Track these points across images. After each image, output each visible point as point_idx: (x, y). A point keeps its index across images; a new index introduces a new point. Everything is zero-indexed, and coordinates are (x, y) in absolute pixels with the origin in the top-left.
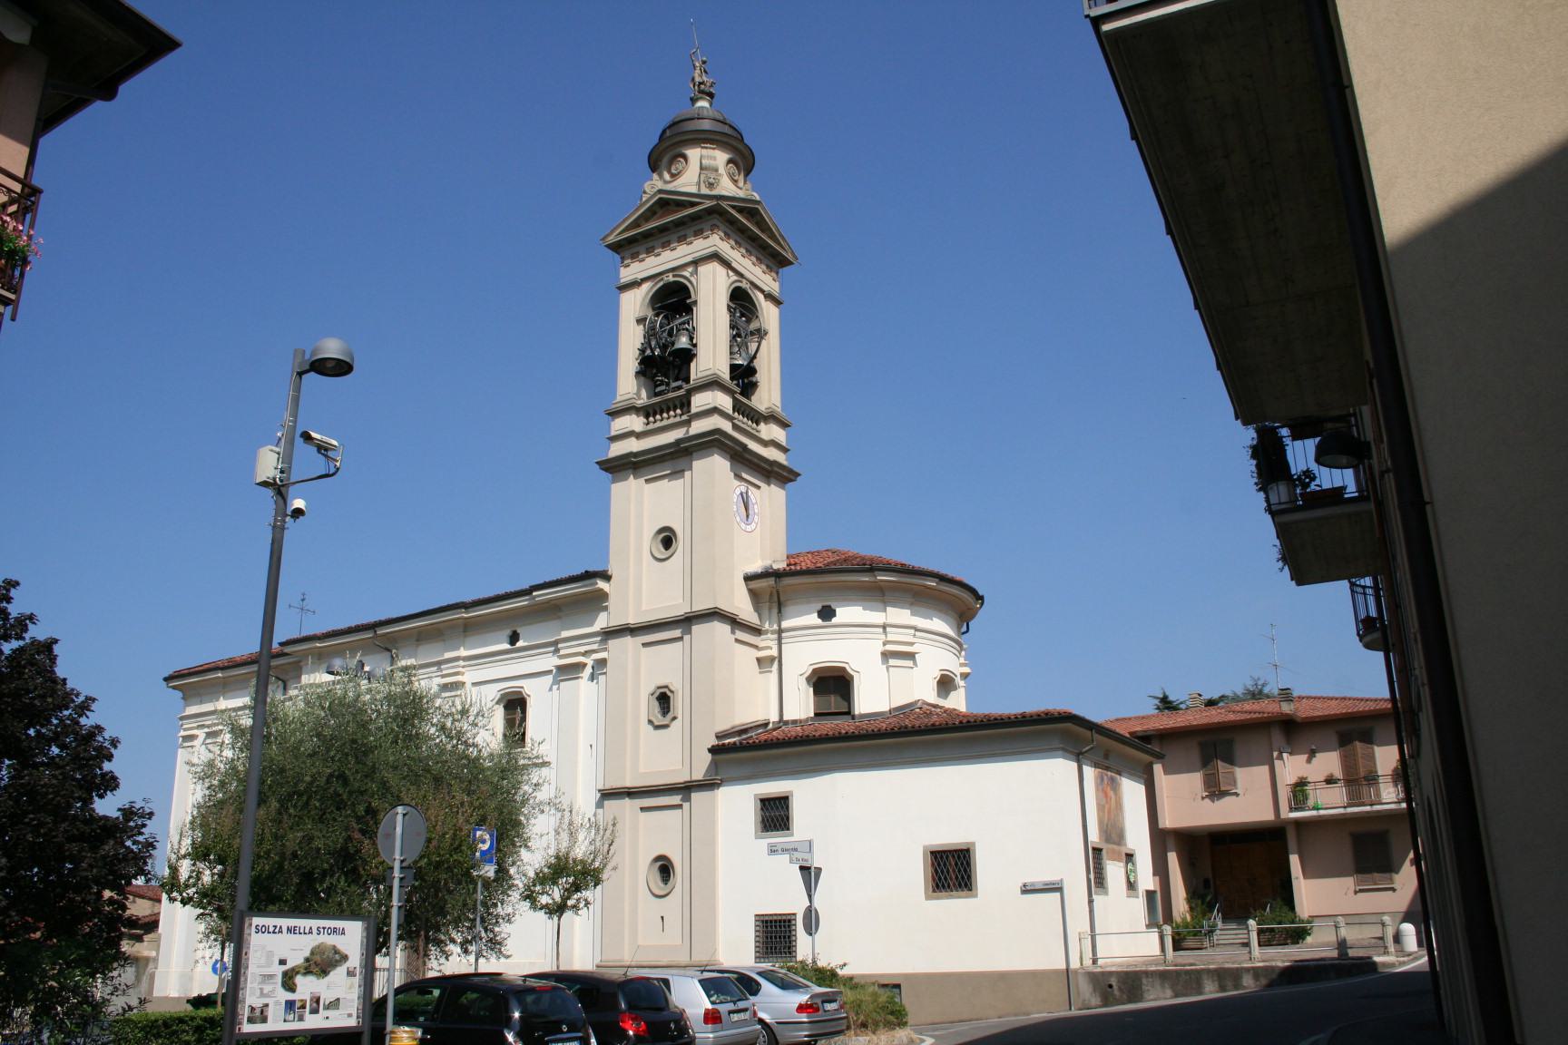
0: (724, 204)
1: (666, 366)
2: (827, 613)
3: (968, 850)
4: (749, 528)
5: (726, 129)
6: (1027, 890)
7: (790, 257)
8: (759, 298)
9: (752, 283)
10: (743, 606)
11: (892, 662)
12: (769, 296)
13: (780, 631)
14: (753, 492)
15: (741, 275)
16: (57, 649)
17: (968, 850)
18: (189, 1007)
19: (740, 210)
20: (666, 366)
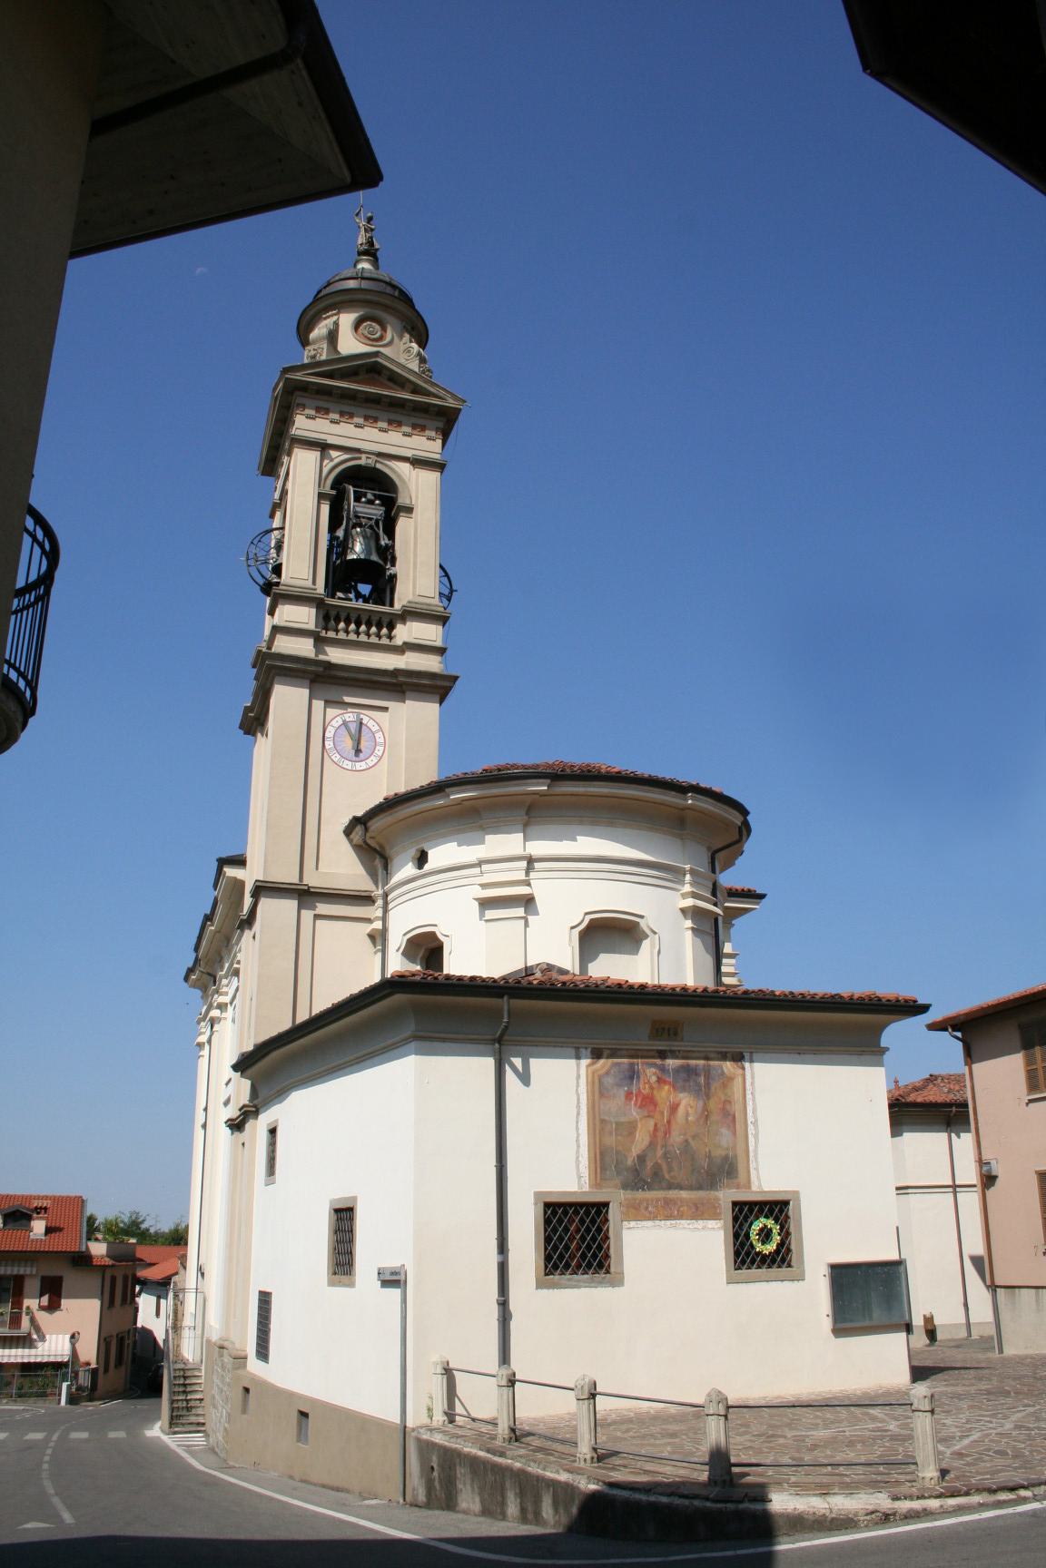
0: (298, 376)
1: (360, 580)
2: (422, 859)
3: (547, 1205)
4: (362, 765)
5: (381, 287)
6: (265, 1299)
7: (451, 403)
8: (402, 472)
9: (380, 455)
10: (340, 865)
11: (490, 914)
12: (417, 462)
13: (386, 895)
14: (368, 718)
15: (358, 451)
16: (198, 993)
17: (547, 1205)
18: (123, 1368)
19: (330, 375)
20: (360, 580)
